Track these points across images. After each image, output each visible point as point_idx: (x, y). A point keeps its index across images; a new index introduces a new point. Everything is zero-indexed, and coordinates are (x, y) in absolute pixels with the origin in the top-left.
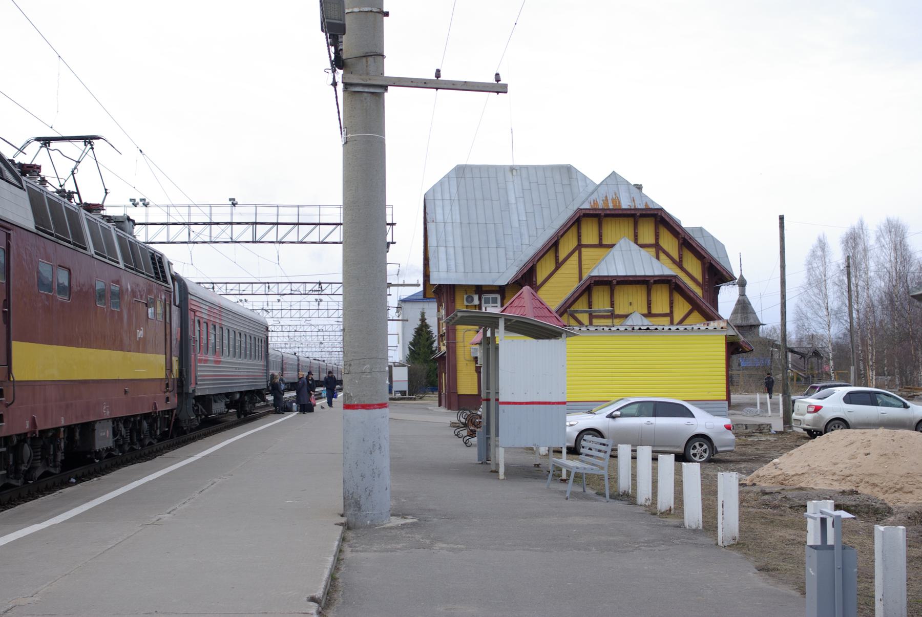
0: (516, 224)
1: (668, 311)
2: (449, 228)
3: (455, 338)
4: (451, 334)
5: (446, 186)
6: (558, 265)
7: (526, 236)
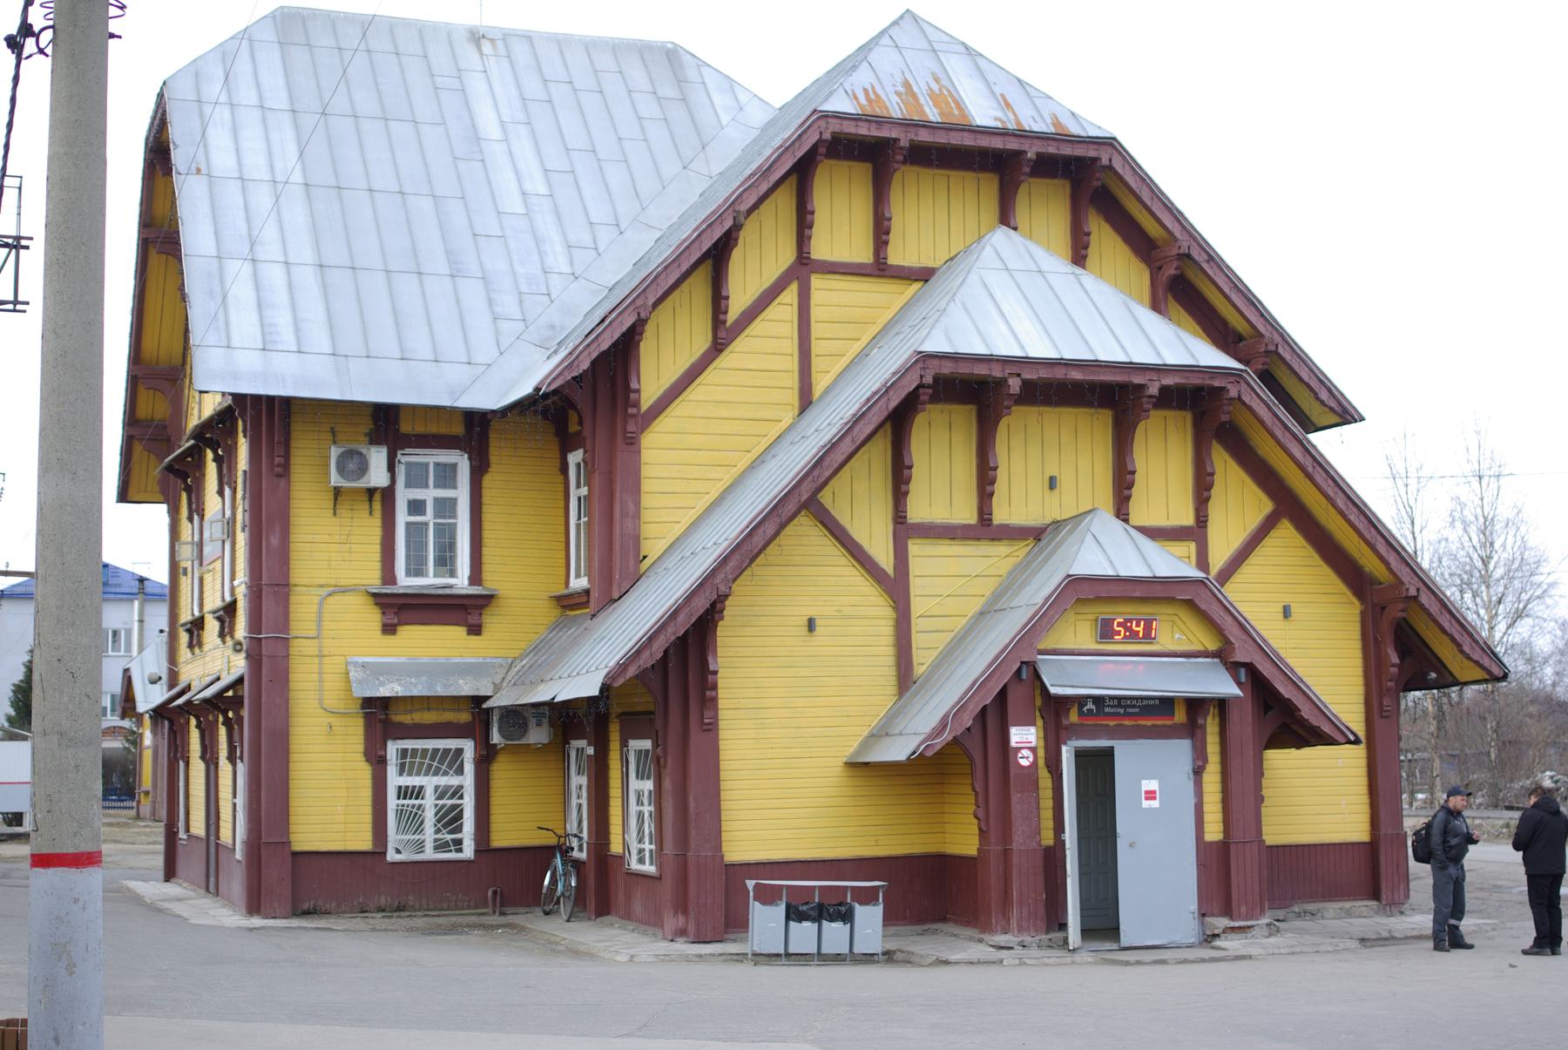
0: (514, 204)
1: (1188, 519)
3: (284, 621)
4: (268, 606)
6: (722, 336)
7: (559, 248)
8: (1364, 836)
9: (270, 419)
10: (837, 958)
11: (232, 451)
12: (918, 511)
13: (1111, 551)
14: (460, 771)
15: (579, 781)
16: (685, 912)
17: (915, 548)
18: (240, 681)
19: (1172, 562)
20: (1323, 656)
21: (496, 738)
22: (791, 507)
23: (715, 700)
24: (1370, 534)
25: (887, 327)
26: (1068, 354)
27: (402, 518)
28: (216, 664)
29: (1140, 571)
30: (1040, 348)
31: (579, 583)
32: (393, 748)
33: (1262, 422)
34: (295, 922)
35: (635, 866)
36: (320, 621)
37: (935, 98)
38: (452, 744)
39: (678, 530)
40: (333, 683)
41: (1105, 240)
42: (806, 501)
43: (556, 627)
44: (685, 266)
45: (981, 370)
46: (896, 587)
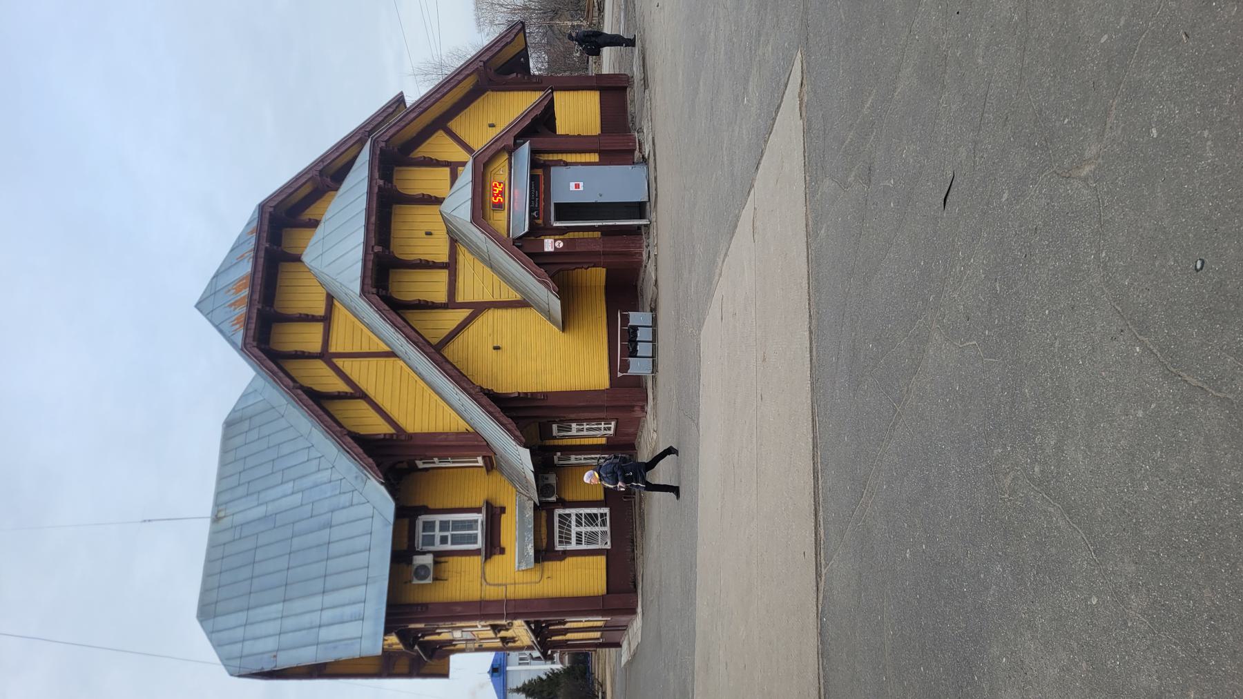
0: (297, 498)
1: (447, 170)
2: (290, 623)
3: (498, 602)
4: (491, 611)
5: (225, 636)
6: (359, 394)
7: (319, 475)
8: (598, 93)
9: (399, 613)
10: (655, 334)
11: (418, 630)
12: (442, 297)
13: (459, 202)
14: (569, 515)
15: (573, 459)
16: (633, 407)
17: (460, 299)
18: (528, 623)
19: (466, 175)
20: (514, 106)
21: (553, 499)
22: (437, 357)
23: (532, 394)
24: (453, 83)
25: (356, 316)
26: (363, 222)
27: (449, 547)
28: (520, 631)
29: (469, 188)
30: (359, 237)
31: (480, 461)
32: (559, 548)
33: (398, 131)
34: (640, 591)
35: (612, 432)
36: (498, 585)
37: (238, 291)
38: (556, 519)
39: (454, 414)
40: (528, 577)
41: (310, 214)
42: (436, 351)
43: (501, 471)
44: (321, 412)
45: (370, 265)
46: (479, 308)
